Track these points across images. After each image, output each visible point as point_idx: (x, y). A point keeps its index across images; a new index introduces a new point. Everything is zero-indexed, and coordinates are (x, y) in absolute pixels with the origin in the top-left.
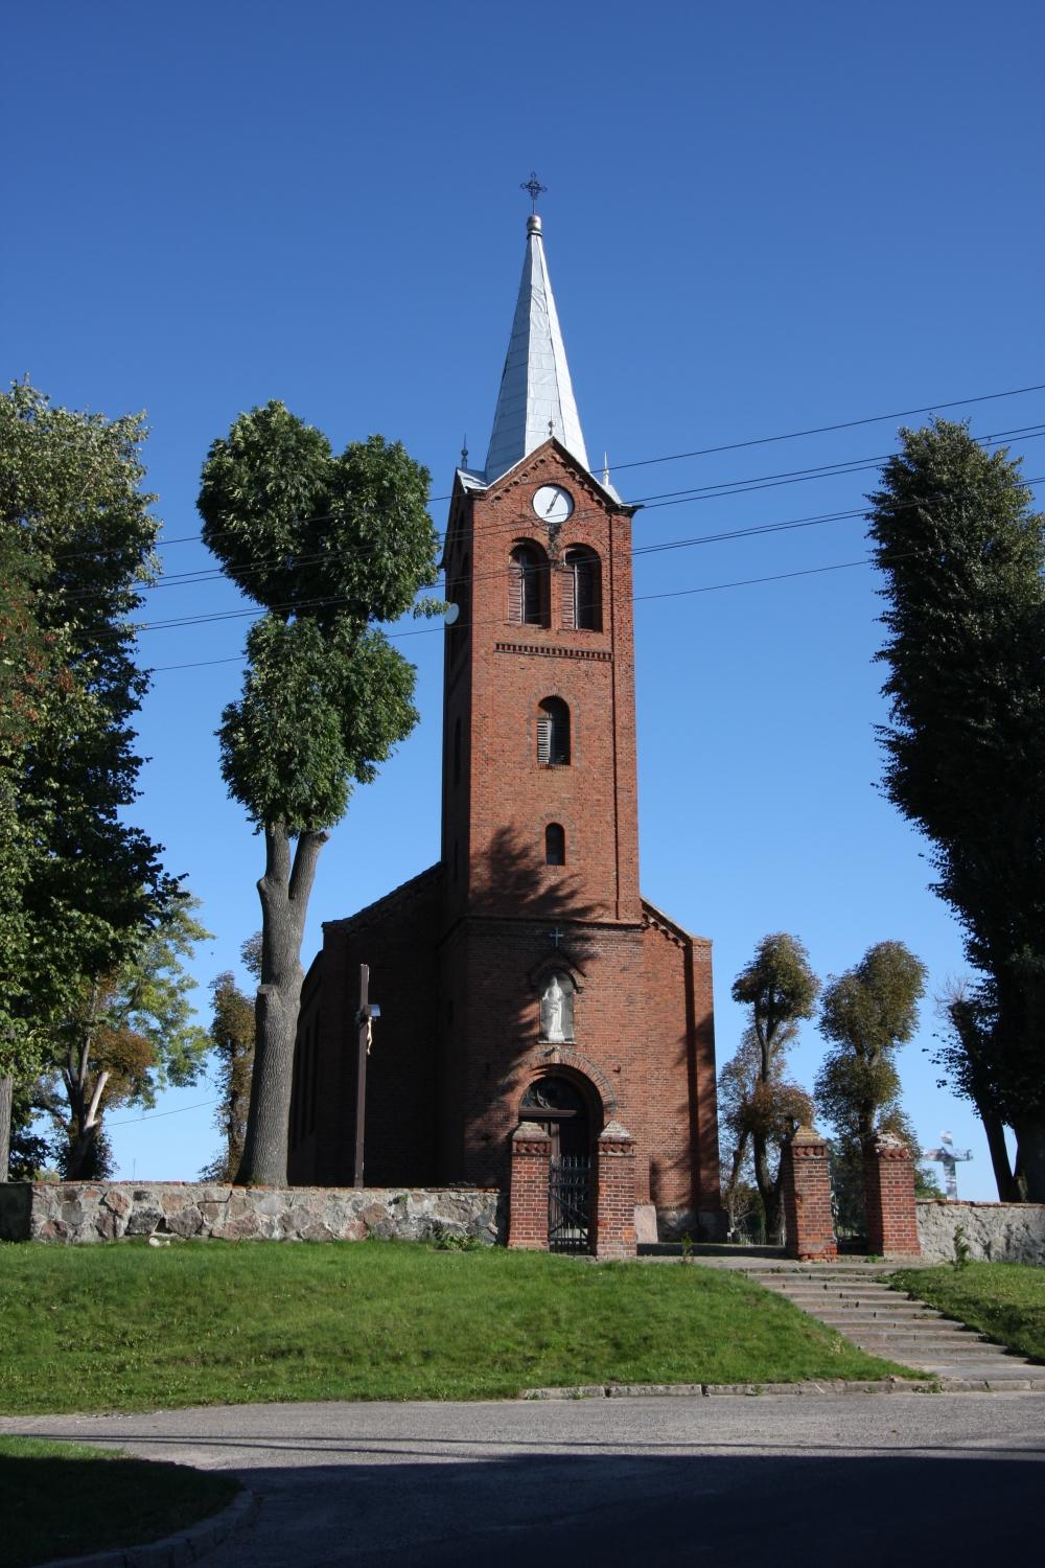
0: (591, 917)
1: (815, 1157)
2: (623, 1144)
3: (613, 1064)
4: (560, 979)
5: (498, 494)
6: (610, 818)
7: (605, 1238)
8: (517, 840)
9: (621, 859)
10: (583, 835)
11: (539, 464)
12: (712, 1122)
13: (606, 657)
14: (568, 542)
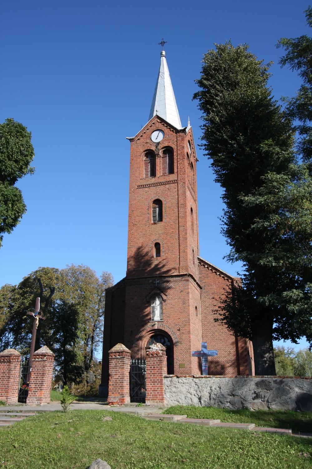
0: (171, 273)
1: (120, 357)
2: (41, 355)
3: (177, 327)
4: (158, 298)
5: (138, 138)
6: (177, 238)
7: (31, 396)
8: (144, 250)
9: (181, 251)
10: (167, 245)
11: (153, 125)
12: (244, 348)
13: (175, 182)
14: (162, 147)
